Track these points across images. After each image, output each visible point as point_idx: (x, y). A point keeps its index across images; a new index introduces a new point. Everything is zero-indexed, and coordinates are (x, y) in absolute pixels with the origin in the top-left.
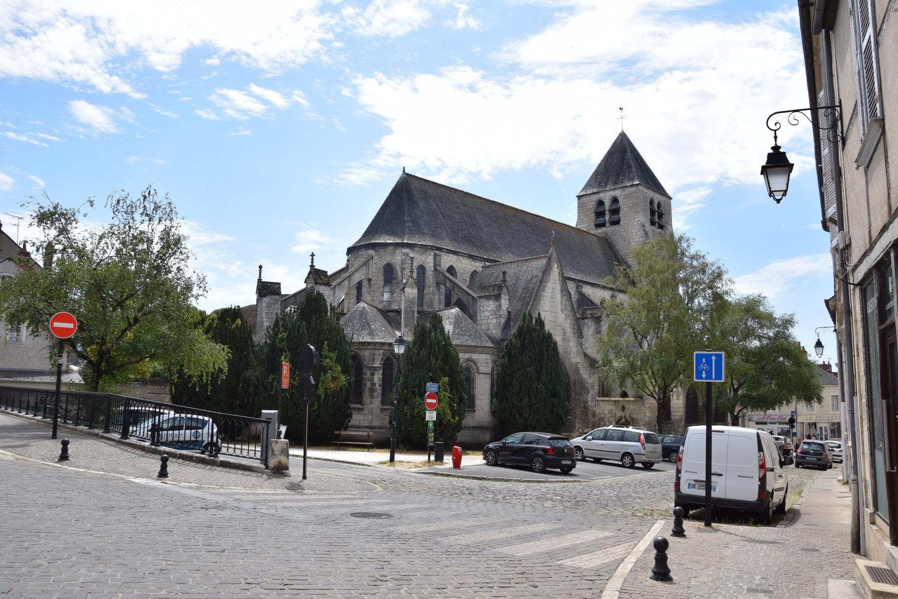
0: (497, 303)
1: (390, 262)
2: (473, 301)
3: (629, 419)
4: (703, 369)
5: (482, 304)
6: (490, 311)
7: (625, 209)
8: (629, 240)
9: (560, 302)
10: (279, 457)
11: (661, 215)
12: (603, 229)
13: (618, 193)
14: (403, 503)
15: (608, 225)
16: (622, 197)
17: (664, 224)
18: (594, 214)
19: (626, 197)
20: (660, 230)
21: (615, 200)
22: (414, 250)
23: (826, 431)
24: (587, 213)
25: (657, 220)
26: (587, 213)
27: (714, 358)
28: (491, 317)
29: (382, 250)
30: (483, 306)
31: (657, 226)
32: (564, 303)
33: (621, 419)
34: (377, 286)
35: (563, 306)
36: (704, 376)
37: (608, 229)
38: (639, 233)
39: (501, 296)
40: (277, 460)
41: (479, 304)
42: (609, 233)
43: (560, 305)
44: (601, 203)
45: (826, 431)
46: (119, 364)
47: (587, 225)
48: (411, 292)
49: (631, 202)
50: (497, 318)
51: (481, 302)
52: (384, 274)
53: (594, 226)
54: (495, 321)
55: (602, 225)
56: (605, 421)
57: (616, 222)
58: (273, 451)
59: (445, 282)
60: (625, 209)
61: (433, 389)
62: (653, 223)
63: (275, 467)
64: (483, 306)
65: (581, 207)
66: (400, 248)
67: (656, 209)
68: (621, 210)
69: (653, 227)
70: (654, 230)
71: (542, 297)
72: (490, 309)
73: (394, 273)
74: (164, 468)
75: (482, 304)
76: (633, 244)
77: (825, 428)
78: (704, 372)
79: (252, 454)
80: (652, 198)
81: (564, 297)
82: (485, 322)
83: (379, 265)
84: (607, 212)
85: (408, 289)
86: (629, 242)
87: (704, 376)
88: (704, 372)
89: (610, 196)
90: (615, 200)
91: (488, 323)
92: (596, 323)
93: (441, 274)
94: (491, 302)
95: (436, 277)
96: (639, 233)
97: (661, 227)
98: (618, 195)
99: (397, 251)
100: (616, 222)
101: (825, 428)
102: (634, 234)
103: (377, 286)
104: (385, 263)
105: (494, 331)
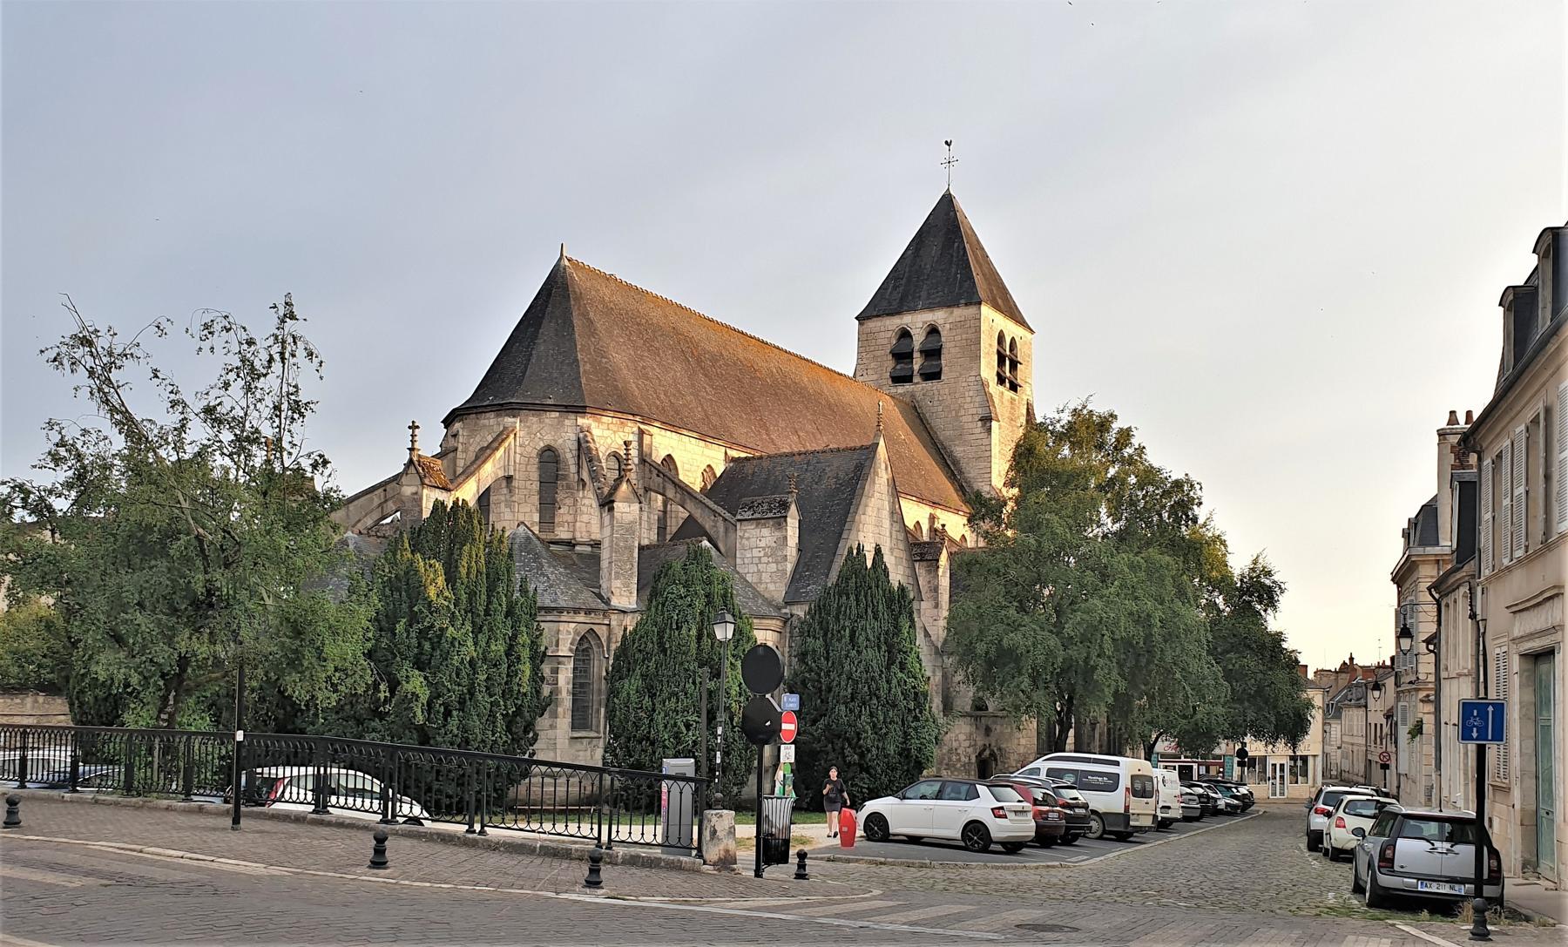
0: (778, 534)
1: (552, 444)
2: (726, 530)
3: (995, 749)
4: (1474, 726)
5: (747, 535)
6: (764, 549)
7: (953, 350)
8: (957, 412)
9: (888, 534)
10: (725, 841)
11: (1014, 365)
12: (908, 387)
13: (939, 317)
14: (512, 886)
15: (916, 379)
16: (948, 326)
17: (1019, 381)
18: (890, 357)
19: (956, 325)
20: (1012, 394)
21: (933, 331)
22: (599, 422)
23: (1282, 769)
24: (878, 353)
25: (1008, 374)
26: (878, 353)
27: (1490, 709)
28: (765, 560)
29: (535, 419)
30: (748, 539)
31: (1008, 385)
32: (894, 536)
33: (984, 750)
34: (526, 492)
35: (894, 541)
36: (1475, 735)
37: (919, 387)
38: (978, 399)
39: (786, 521)
40: (721, 847)
41: (739, 533)
42: (919, 396)
43: (888, 539)
44: (905, 334)
45: (1282, 769)
46: (366, 674)
47: (875, 377)
48: (627, 510)
49: (964, 336)
50: (777, 563)
51: (745, 531)
52: (540, 468)
53: (890, 382)
54: (773, 567)
55: (907, 379)
56: (958, 754)
57: (933, 375)
58: (714, 832)
59: (664, 488)
60: (953, 350)
61: (791, 705)
62: (1001, 380)
63: (720, 859)
64: (748, 539)
65: (864, 341)
66: (572, 416)
67: (1008, 353)
68: (944, 351)
69: (1001, 388)
70: (1002, 393)
71: (861, 526)
72: (762, 544)
73: (562, 466)
74: (380, 851)
75: (747, 535)
76: (964, 419)
77: (1282, 766)
78: (1475, 729)
79: (649, 838)
80: (1002, 331)
81: (895, 524)
82: (753, 568)
83: (529, 449)
84: (916, 355)
85: (620, 504)
86: (957, 416)
87: (1475, 735)
88: (1475, 729)
89: (925, 323)
90: (933, 331)
91: (759, 571)
92: (929, 572)
93: (655, 472)
94: (765, 532)
95: (644, 478)
96: (978, 399)
97: (1014, 387)
98: (941, 321)
99: (567, 422)
100: (933, 375)
101: (1282, 766)
102: (968, 400)
103: (526, 492)
104: (542, 445)
105: (771, 587)
